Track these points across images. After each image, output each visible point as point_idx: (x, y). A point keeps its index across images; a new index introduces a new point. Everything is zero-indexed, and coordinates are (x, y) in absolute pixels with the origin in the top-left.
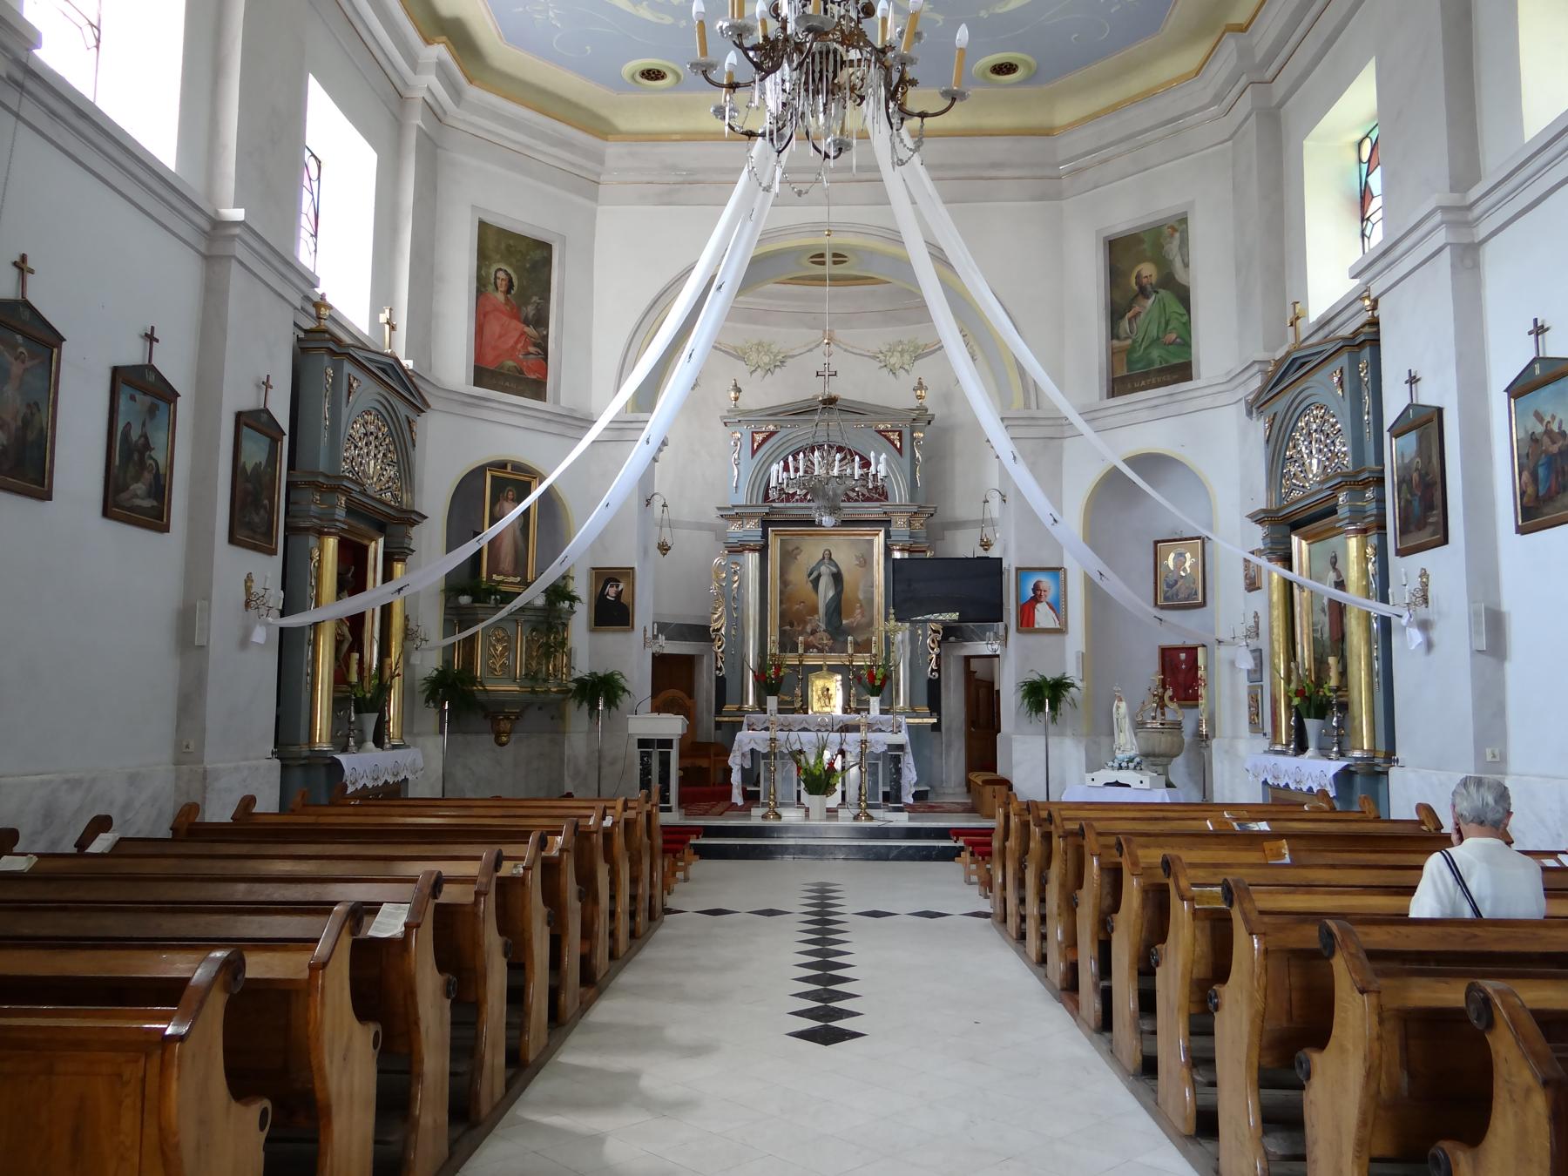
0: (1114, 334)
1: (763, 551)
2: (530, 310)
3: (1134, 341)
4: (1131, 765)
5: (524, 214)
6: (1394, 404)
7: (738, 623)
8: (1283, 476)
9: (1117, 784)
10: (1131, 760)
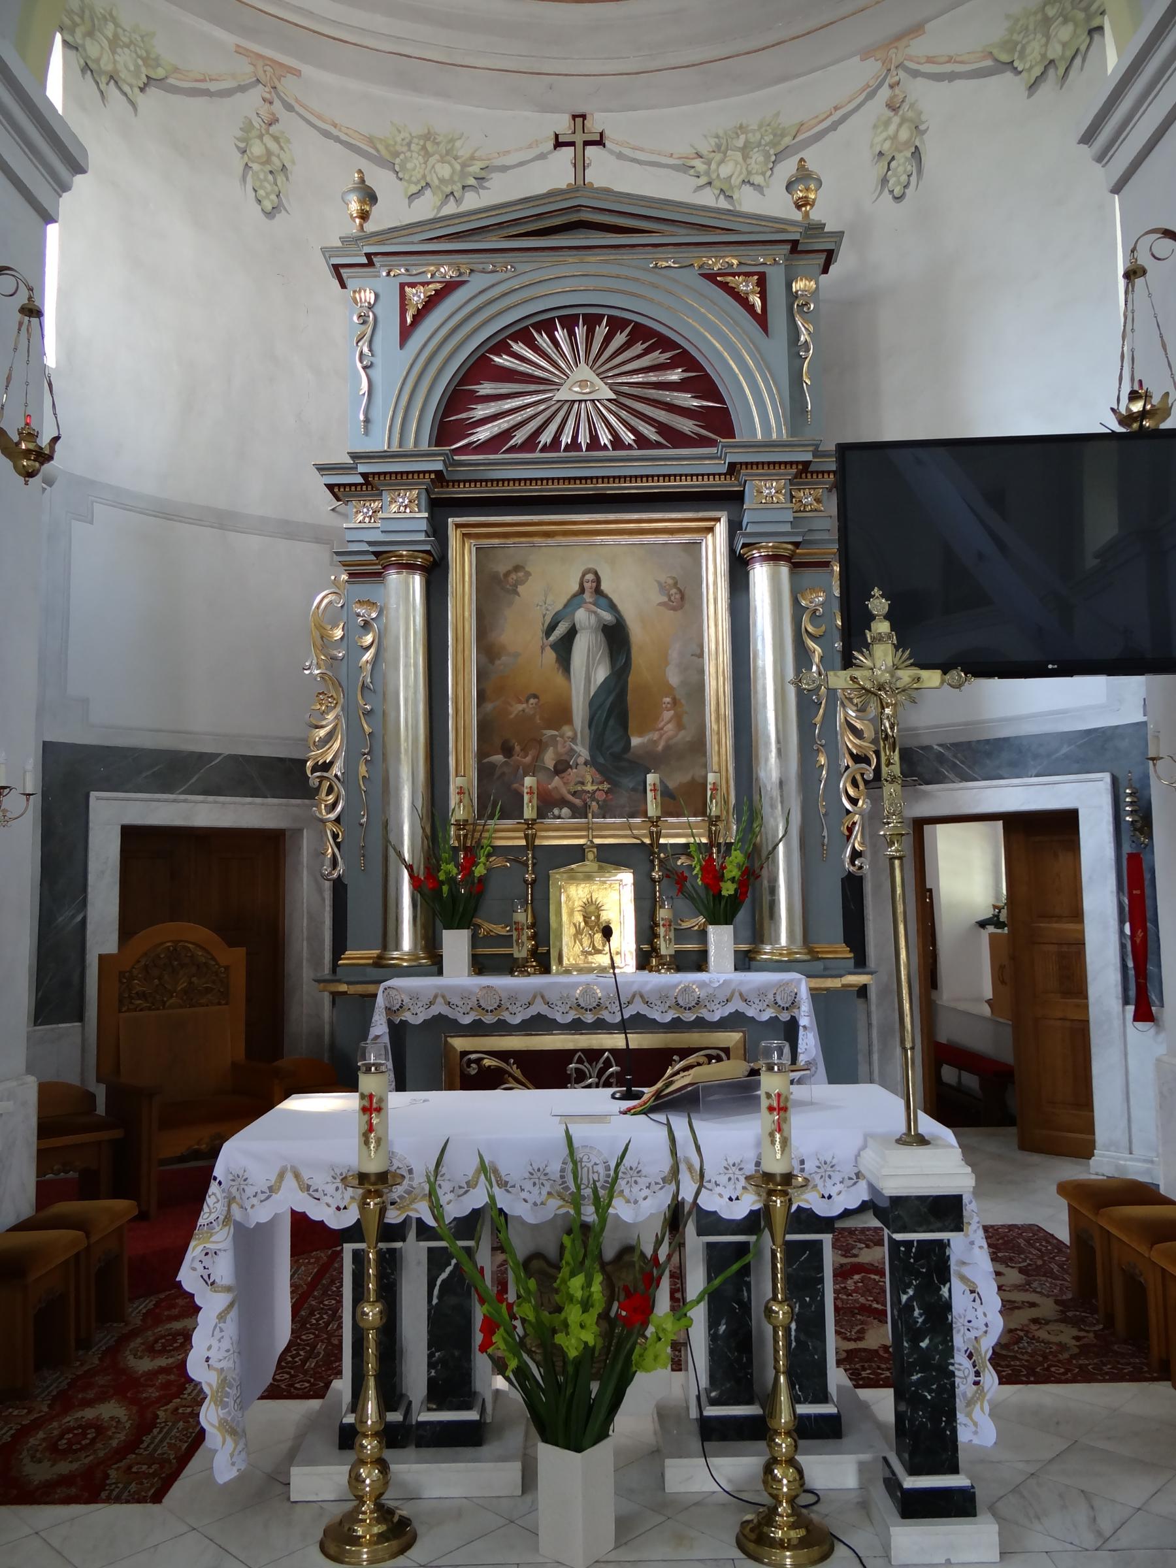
1: (435, 571)
7: (371, 746)
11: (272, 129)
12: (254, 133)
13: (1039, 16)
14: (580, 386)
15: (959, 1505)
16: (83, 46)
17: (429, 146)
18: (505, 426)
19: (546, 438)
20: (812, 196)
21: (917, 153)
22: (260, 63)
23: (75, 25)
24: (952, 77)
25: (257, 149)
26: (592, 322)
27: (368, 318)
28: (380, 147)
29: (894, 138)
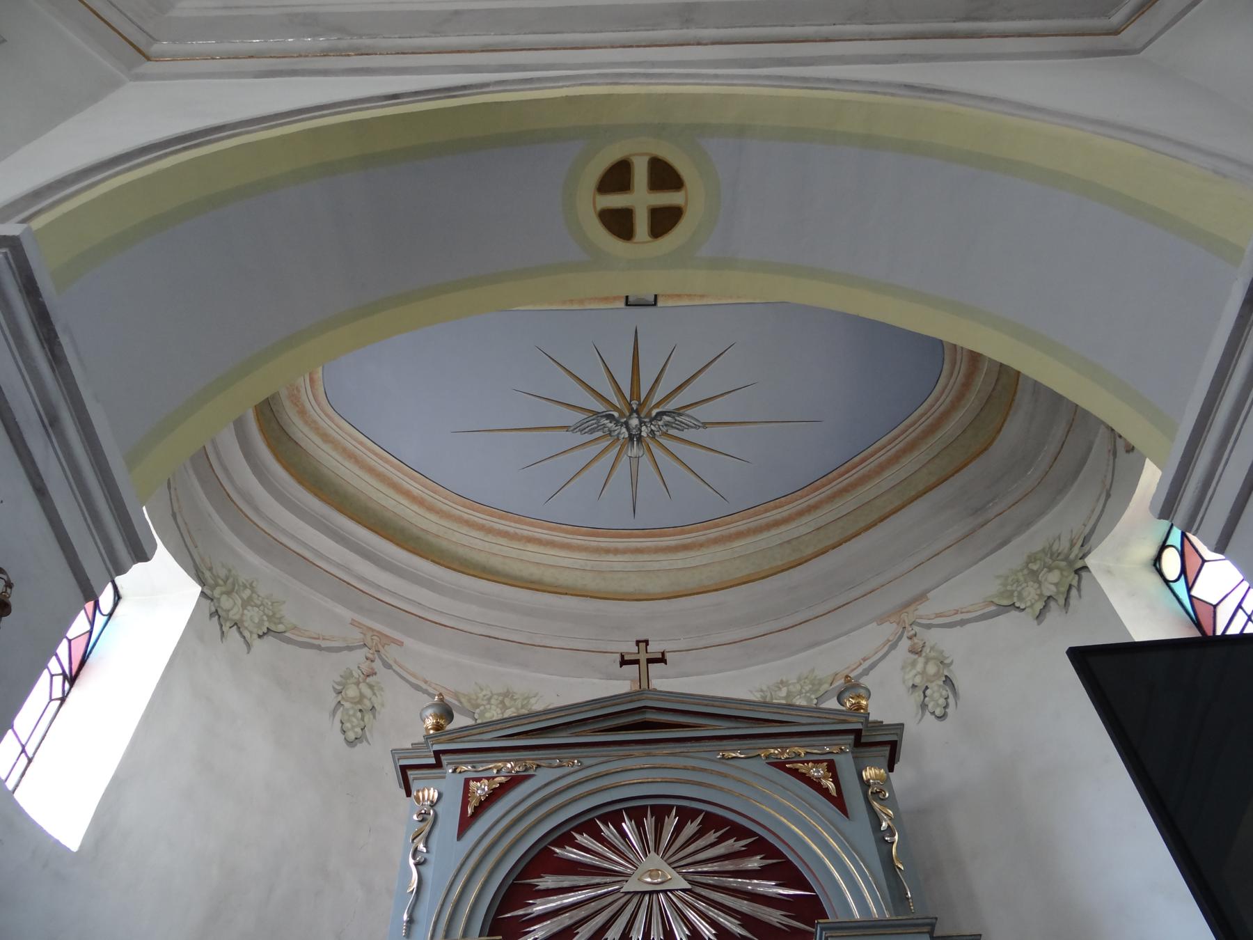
11: (369, 680)
12: (353, 680)
13: (1026, 572)
14: (650, 876)
16: (219, 599)
17: (507, 702)
18: (568, 922)
20: (864, 702)
21: (948, 681)
22: (369, 634)
23: (217, 585)
24: (962, 623)
25: (352, 692)
26: (660, 813)
27: (429, 819)
28: (463, 700)
29: (923, 673)
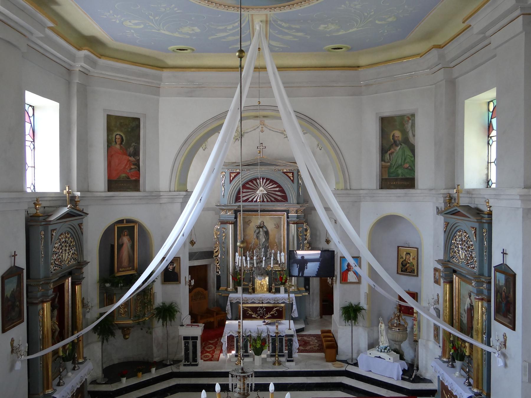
0: (383, 159)
1: (235, 224)
2: (131, 149)
3: (391, 164)
4: (386, 351)
5: (125, 108)
6: (497, 260)
8: (450, 249)
9: (380, 357)
10: (386, 348)
15: (292, 361)
19: (255, 200)
